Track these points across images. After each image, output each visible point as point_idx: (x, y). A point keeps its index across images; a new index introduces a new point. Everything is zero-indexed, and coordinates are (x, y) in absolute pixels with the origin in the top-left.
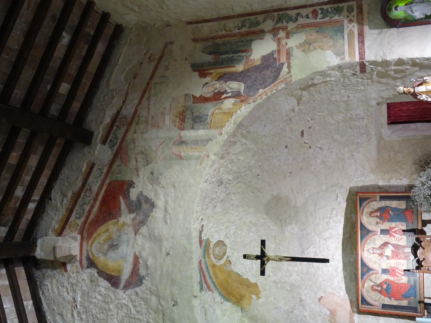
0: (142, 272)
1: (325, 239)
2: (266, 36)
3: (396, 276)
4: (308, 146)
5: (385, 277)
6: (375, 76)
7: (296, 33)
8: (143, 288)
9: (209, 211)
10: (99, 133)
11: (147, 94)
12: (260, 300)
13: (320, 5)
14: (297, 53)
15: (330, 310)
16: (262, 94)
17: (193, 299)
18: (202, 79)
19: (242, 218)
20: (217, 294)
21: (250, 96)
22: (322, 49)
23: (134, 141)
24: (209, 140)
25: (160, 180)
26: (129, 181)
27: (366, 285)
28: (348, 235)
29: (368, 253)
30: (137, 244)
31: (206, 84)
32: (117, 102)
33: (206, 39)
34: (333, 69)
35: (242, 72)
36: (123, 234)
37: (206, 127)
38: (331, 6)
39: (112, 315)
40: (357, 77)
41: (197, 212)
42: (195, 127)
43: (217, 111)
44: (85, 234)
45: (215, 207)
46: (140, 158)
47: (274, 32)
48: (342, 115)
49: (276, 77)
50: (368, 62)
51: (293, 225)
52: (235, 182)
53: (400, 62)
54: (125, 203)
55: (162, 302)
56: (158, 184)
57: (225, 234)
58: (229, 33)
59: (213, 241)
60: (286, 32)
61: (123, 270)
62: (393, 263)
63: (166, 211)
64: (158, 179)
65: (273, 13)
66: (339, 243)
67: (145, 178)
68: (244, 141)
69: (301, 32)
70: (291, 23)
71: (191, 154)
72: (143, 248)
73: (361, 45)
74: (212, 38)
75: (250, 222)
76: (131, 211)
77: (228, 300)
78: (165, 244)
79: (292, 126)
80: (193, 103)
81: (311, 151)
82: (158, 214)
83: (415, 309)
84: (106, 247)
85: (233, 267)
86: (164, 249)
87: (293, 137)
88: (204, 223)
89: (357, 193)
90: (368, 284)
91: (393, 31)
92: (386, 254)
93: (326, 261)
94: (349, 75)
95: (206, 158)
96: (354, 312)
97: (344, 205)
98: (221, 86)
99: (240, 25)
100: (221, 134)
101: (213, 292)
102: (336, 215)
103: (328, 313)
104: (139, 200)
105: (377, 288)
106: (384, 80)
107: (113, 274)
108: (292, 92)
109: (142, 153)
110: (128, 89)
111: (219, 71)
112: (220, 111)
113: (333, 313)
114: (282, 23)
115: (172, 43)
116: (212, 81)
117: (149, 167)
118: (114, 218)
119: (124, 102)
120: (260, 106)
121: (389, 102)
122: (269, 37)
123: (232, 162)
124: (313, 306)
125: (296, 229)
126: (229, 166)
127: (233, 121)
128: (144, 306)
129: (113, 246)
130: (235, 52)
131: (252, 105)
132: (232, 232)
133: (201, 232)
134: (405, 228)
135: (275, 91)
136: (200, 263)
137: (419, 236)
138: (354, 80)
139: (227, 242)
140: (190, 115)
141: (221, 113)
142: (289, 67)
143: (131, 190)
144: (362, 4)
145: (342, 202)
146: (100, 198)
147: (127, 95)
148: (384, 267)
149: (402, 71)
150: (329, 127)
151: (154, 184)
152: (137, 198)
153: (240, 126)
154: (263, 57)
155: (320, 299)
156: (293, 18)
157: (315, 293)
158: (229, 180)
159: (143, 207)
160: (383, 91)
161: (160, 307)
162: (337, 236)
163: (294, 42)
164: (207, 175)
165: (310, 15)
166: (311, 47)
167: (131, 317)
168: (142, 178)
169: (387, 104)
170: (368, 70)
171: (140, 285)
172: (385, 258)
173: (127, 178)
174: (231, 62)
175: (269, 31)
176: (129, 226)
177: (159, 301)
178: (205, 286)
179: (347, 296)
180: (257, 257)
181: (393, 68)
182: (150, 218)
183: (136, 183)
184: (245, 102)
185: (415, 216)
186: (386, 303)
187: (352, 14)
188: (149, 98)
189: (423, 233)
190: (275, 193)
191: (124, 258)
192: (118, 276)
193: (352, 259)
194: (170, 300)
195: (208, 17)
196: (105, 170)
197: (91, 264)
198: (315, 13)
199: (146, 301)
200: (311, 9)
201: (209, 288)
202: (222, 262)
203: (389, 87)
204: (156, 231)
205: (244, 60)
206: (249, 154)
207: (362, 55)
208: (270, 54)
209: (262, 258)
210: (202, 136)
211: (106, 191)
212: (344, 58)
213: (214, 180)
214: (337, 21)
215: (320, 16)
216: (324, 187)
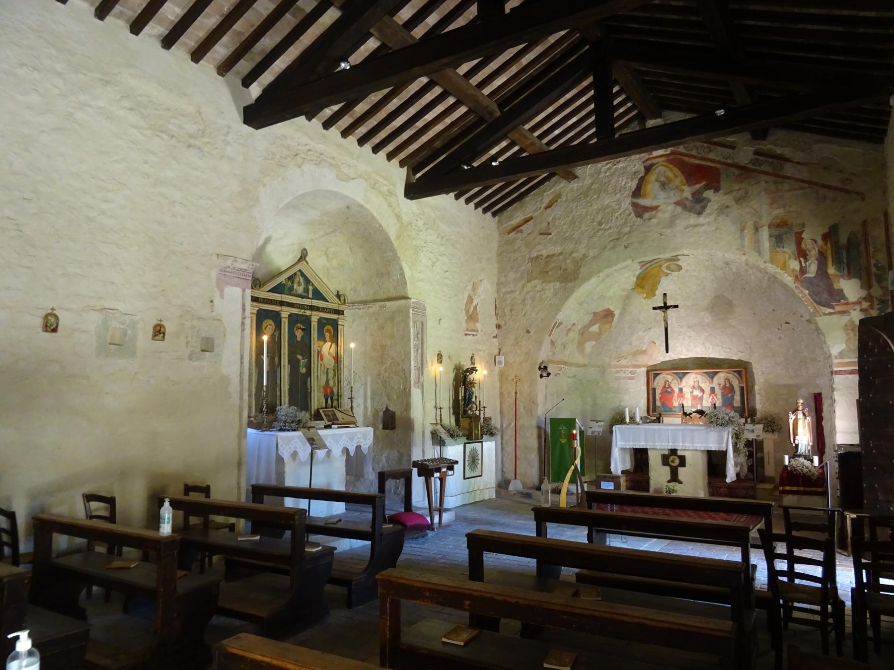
0: (646, 215)
8: (635, 219)
10: (765, 146)
14: (845, 319)
23: (758, 183)
24: (759, 252)
29: (693, 378)
31: (815, 242)
32: (799, 156)
33: (865, 234)
35: (827, 273)
44: (671, 157)
46: (741, 192)
49: (820, 304)
56: (718, 215)
59: (679, 263)
62: (688, 396)
63: (696, 226)
64: (723, 213)
71: (746, 239)
72: (664, 212)
74: (866, 240)
76: (693, 195)
77: (637, 279)
82: (693, 219)
83: (654, 410)
84: (663, 179)
90: (670, 378)
97: (735, 358)
100: (765, 262)
102: (726, 352)
104: (704, 199)
111: (829, 252)
113: (644, 352)
115: (863, 199)
117: (734, 203)
118: (687, 180)
119: (798, 163)
120: (794, 295)
122: (864, 293)
129: (663, 186)
140: (782, 231)
142: (830, 314)
146: (703, 163)
154: (842, 291)
159: (698, 204)
174: (838, 262)
180: (665, 303)
188: (801, 188)
190: (734, 302)
191: (655, 197)
196: (729, 161)
197: (648, 169)
199: (625, 224)
202: (665, 270)
204: (677, 222)
205: (839, 274)
207: (837, 373)
211: (710, 167)
216: (749, 341)
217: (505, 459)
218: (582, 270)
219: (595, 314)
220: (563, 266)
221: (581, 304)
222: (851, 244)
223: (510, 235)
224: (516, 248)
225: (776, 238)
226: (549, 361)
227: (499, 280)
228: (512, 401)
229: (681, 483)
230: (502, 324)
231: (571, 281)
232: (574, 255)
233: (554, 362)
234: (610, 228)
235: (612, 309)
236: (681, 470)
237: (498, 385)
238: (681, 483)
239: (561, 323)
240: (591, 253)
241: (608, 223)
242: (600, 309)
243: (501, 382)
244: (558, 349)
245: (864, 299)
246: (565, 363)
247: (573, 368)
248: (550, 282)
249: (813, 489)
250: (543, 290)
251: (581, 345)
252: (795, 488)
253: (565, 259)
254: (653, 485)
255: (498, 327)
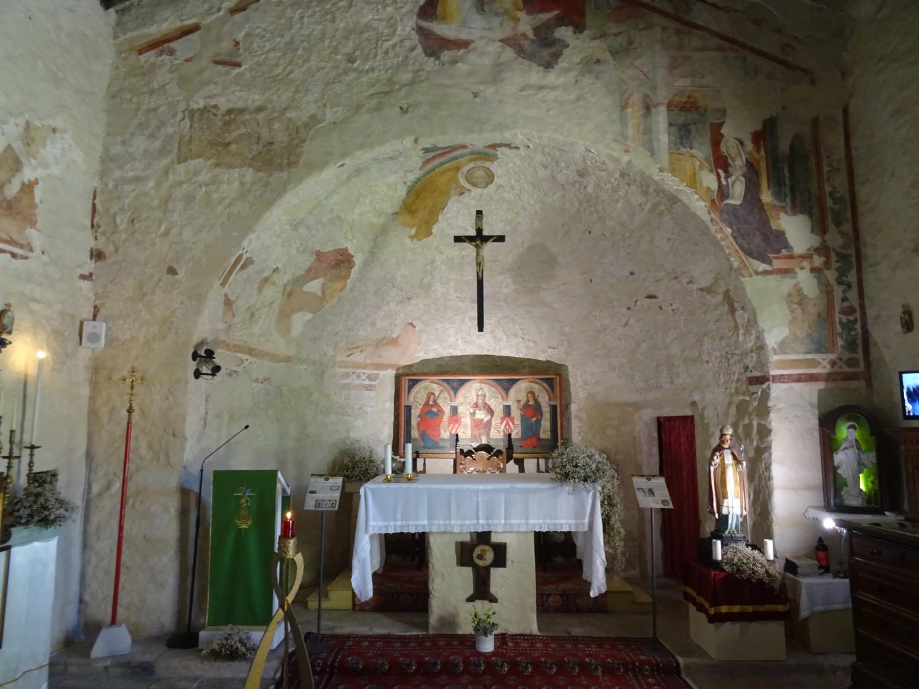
0: (446, 55)
1: (493, 331)
2: (817, 237)
3: (449, 424)
4: (632, 305)
5: (447, 410)
6: (741, 398)
7: (819, 282)
9: (539, 157)
11: (726, 44)
12: (409, 240)
13: (862, 318)
14: (787, 284)
15: (397, 338)
16: (724, 233)
17: (413, 138)
18: (751, 136)
19: (525, 210)
20: (417, 176)
21: (721, 215)
22: (791, 322)
23: (650, 27)
24: (652, 151)
25: (587, 76)
26: (585, 24)
27: (434, 386)
28: (499, 363)
29: (477, 389)
30: (486, 44)
31: (742, 143)
33: (816, 141)
34: (758, 338)
35: (760, 200)
36: (501, 19)
37: (672, 145)
38: (860, 335)
39: (378, 11)
40: (740, 374)
41: (540, 138)
42: (673, 129)
43: (698, 163)
45: (545, 167)
47: (823, 250)
48: (679, 354)
49: (749, 254)
50: (769, 388)
51: (512, 287)
52: (581, 197)
53: (765, 432)
54: (548, 20)
55: (404, 91)
56: (582, 73)
57: (503, 184)
58: (825, 177)
59: (494, 167)
60: (822, 267)
61: (446, 23)
62: (467, 420)
63: (541, 88)
64: (590, 71)
65: (853, 247)
66: (488, 351)
67: (590, 51)
68: (647, 207)
69: (821, 292)
70: (837, 274)
71: (630, 124)
73: (796, 378)
74: (817, 152)
75: (519, 222)
76: (537, 30)
77: (409, 192)
78: (490, 90)
79: (666, 280)
80: (711, 124)
81: (624, 310)
82: (536, 75)
85: (454, 198)
86: (482, 88)
87: (647, 283)
88: (522, 151)
89: (560, 375)
90: (436, 389)
91: (814, 422)
92: (477, 412)
93: (481, 328)
94: (745, 361)
95: (624, 148)
96: (398, 369)
97: (542, 357)
98: (738, 168)
99: (837, 195)
100: (661, 170)
101: (421, 168)
102: (527, 347)
103: (395, 336)
105: (431, 400)
106: (733, 410)
107: (439, 8)
108: (723, 278)
109: (631, 43)
110: (735, 11)
112: (697, 168)
113: (394, 342)
114: (837, 262)
115: (813, 82)
116: (745, 154)
117: (608, 56)
120: (705, 231)
121: (697, 418)
122: (815, 241)
123: (615, 190)
124: (402, 315)
125: (506, 291)
126: (609, 186)
127: (681, 188)
128: (396, 61)
130: (793, 189)
131: (706, 218)
132: (506, 195)
133: (508, 146)
134: (513, 436)
135: (727, 252)
136: (464, 147)
137: (505, 454)
138: (737, 368)
139: (492, 188)
140: (692, 119)
141: (694, 169)
142: (765, 273)
143: (570, 28)
144: (859, 379)
145: (546, 354)
147: (726, 10)
148: (461, 409)
149: (748, 435)
150: (660, 335)
151: (581, 66)
152: (559, 39)
153: (674, 199)
155: (411, 324)
156: (844, 278)
157: (419, 319)
158: (585, 187)
159: (544, 49)
160: (716, 409)
161: (397, 87)
162: (498, 348)
163: (805, 280)
164: (597, 150)
165: (846, 304)
166: (795, 306)
167: (377, 41)
168: (591, 45)
169: (692, 418)
170: (752, 388)
171: (426, 53)
172: (472, 411)
173: (589, 20)
174: (776, 183)
175: (824, 242)
176: (514, 29)
177: (406, 85)
178: (430, 155)
179: (418, 361)
180: (479, 231)
181: (755, 423)
182: (527, 63)
183: (581, 36)
184: (712, 205)
185: (530, 450)
186: (413, 411)
187: (844, 366)
188: (720, 49)
189: (509, 458)
190: (560, 259)
191: (464, 24)
192: (436, 16)
193: (466, 368)
194: (409, 101)
195: (854, 142)
198: (849, 311)
200: (856, 304)
201: (427, 162)
202: (463, 182)
203: (721, 417)
204: (508, 75)
205: (778, 204)
206: (625, 217)
207: (780, 379)
208: (788, 243)
209: (479, 238)
210: (658, 141)
212: (775, 353)
213: (589, 163)
214: (834, 343)
215: (844, 319)
216: (567, 329)
217: (90, 570)
218: (306, 147)
219: (319, 254)
220: (265, 135)
221: (295, 226)
222: (796, 156)
223: (143, 58)
224: (155, 85)
225: (680, 129)
226: (217, 342)
227: (106, 150)
228: (121, 431)
229: (493, 600)
230: (109, 250)
231: (281, 168)
232: (291, 114)
233: (227, 346)
234: (373, 69)
235: (351, 251)
236: (496, 574)
237: (85, 391)
238: (493, 600)
239: (249, 262)
240: (329, 115)
241: (366, 59)
242: (329, 248)
243: (94, 385)
244: (237, 320)
245: (817, 250)
246: (251, 351)
247: (266, 363)
248: (232, 167)
249: (767, 607)
250: (215, 181)
251: (285, 316)
252: (736, 609)
253: (270, 122)
254: (437, 606)
255: (97, 255)
